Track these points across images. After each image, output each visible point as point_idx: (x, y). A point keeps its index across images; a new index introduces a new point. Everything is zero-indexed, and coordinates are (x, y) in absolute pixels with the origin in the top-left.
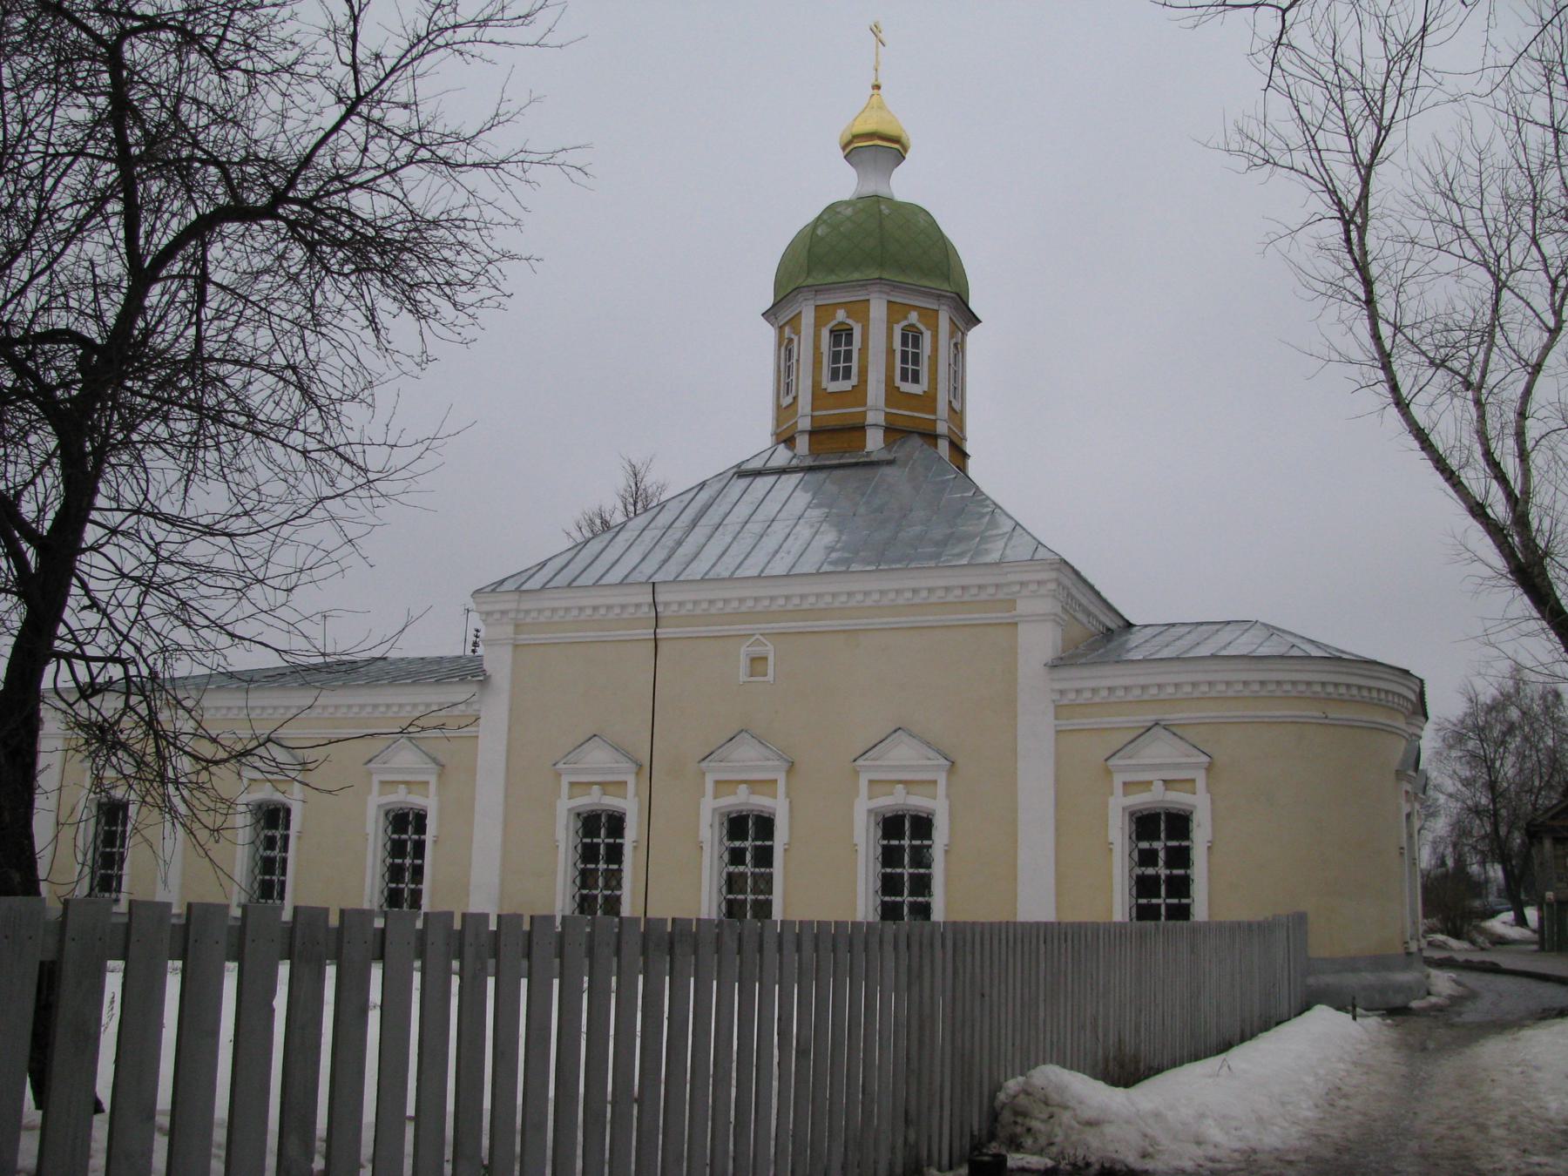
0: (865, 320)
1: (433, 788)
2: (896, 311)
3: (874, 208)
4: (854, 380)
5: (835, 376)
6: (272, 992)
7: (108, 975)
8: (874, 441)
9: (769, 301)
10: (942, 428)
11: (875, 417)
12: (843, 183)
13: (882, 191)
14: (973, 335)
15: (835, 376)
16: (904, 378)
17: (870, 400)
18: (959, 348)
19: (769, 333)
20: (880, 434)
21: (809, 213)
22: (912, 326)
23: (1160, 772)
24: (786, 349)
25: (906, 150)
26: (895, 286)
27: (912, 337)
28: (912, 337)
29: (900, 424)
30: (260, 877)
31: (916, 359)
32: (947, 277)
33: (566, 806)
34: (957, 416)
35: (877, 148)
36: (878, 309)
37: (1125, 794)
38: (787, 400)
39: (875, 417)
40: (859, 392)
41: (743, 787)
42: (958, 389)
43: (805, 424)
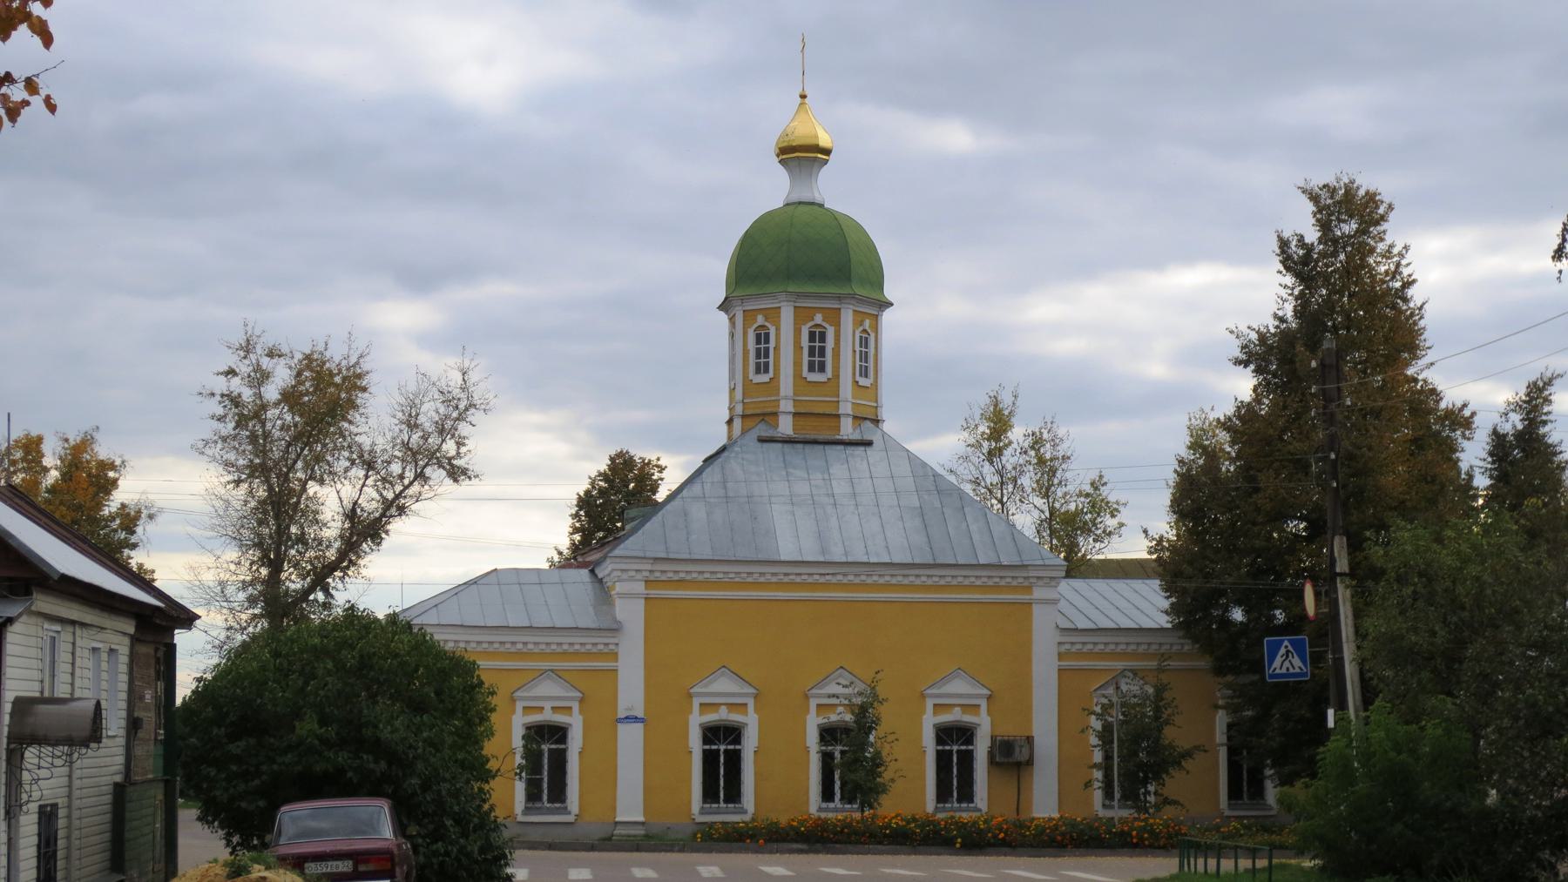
1: (751, 708)
2: (801, 315)
3: (802, 211)
4: (771, 374)
5: (758, 371)
8: (786, 426)
11: (786, 406)
12: (772, 189)
15: (758, 371)
16: (811, 368)
17: (783, 393)
20: (790, 419)
21: (14, 532)
23: (721, 694)
26: (799, 295)
27: (817, 336)
28: (817, 336)
30: (722, 805)
31: (822, 352)
33: (696, 722)
35: (801, 156)
37: (935, 713)
39: (786, 406)
40: (775, 380)
41: (958, 709)
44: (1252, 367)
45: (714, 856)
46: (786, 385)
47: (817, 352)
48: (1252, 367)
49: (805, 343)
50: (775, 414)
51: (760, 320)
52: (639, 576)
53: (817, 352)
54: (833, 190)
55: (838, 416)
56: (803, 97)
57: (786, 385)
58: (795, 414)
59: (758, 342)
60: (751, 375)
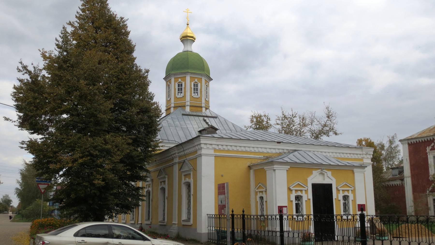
0: (185, 81)
4: (182, 95)
6: (95, 220)
7: (204, 159)
8: (188, 109)
9: (164, 76)
10: (203, 105)
12: (180, 48)
13: (189, 49)
14: (211, 83)
18: (207, 86)
19: (164, 82)
22: (196, 82)
24: (168, 86)
25: (195, 39)
26: (192, 73)
27: (196, 85)
28: (196, 85)
29: (147, 218)
32: (203, 70)
34: (207, 102)
35: (186, 39)
36: (188, 78)
38: (169, 99)
39: (188, 103)
40: (184, 96)
42: (207, 96)
43: (173, 105)
44: (15, 91)
45: (407, 154)
46: (188, 98)
47: (196, 90)
48: (15, 91)
49: (193, 87)
50: (185, 106)
51: (180, 80)
52: (210, 147)
53: (196, 90)
54: (195, 48)
55: (202, 107)
56: (188, 24)
57: (188, 98)
58: (190, 106)
59: (179, 86)
60: (177, 95)
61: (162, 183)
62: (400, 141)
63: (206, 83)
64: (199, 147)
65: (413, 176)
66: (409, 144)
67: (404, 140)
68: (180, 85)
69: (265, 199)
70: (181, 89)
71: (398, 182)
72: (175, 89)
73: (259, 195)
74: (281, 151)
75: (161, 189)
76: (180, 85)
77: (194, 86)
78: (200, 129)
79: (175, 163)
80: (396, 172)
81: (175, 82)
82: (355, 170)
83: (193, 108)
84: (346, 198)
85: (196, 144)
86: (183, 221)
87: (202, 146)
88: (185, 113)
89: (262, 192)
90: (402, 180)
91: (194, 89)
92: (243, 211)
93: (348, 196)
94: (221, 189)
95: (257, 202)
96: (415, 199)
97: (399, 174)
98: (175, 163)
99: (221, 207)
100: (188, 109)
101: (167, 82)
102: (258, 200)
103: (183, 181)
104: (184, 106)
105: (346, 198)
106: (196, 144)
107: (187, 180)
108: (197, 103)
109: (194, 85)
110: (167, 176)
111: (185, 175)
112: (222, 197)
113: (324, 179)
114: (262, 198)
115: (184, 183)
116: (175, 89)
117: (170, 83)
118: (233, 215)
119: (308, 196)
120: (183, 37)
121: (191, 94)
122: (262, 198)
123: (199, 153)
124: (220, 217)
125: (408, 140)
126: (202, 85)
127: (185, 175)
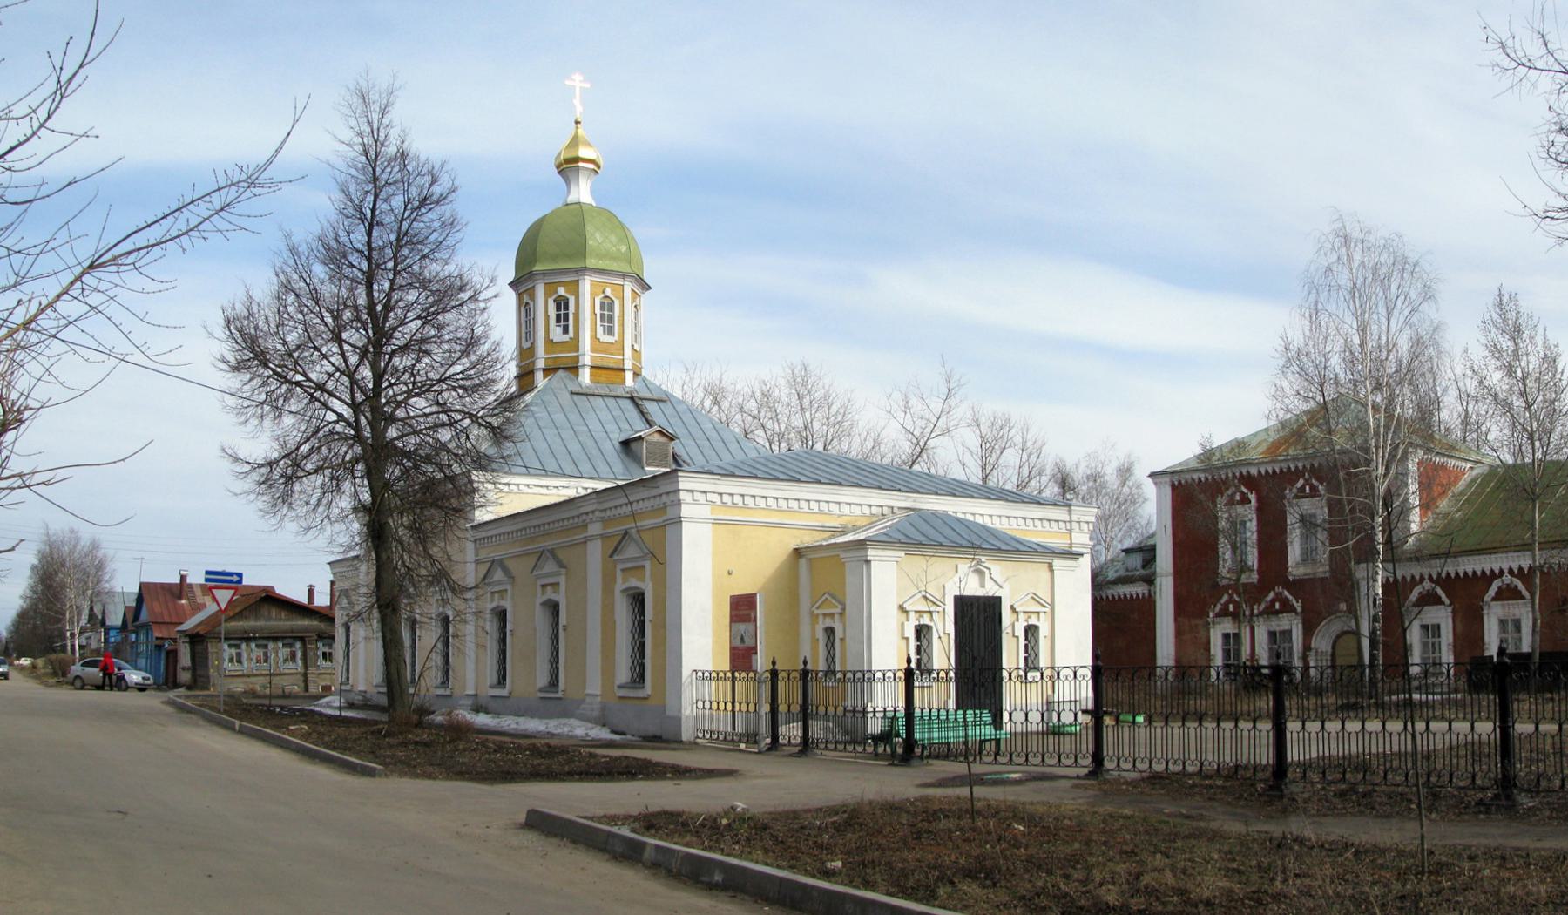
7: (687, 529)
9: (511, 276)
10: (628, 365)
14: (646, 297)
28: (608, 305)
38: (526, 345)
43: (541, 364)
49: (598, 311)
59: (558, 308)
61: (549, 589)
62: (1152, 475)
63: (634, 300)
64: (672, 497)
65: (1178, 573)
66: (1173, 486)
67: (1163, 473)
68: (562, 304)
69: (839, 634)
70: (566, 316)
71: (1139, 589)
72: (547, 317)
73: (821, 625)
74: (875, 510)
75: (543, 604)
76: (562, 304)
77: (602, 308)
78: (623, 437)
79: (593, 538)
80: (1136, 560)
81: (547, 295)
82: (1057, 562)
83: (604, 375)
84: (1031, 631)
85: (663, 489)
86: (620, 687)
87: (683, 495)
88: (577, 389)
89: (832, 615)
90: (1150, 580)
91: (602, 316)
92: (774, 663)
93: (1036, 628)
94: (742, 608)
95: (815, 641)
96: (1179, 633)
97: (1144, 567)
98: (593, 538)
99: (741, 657)
100: (585, 376)
101: (520, 295)
102: (821, 635)
103: (619, 585)
104: (574, 369)
105: (1031, 631)
106: (663, 489)
107: (634, 582)
108: (610, 359)
109: (602, 304)
110: (563, 571)
111: (623, 570)
112: (742, 627)
113: (982, 585)
114: (830, 632)
115: (624, 591)
116: (547, 317)
117: (532, 297)
118: (774, 674)
119: (944, 626)
120: (567, 161)
121: (594, 330)
122: (830, 632)
123: (670, 514)
124: (734, 678)
125: (1172, 473)
126: (625, 308)
127: (623, 570)
